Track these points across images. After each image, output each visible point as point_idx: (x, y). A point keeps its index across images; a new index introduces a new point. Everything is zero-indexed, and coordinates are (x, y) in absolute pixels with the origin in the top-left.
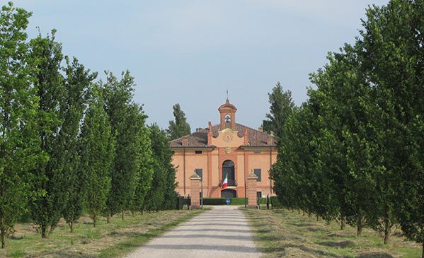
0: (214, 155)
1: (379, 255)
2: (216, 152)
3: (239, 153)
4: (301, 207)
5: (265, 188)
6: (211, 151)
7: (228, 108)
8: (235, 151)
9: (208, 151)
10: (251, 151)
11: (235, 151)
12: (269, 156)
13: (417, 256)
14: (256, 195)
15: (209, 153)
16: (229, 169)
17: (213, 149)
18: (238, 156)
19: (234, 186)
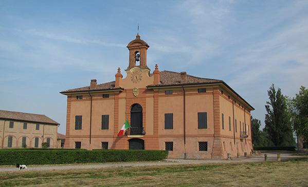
0: (121, 98)
1: (64, 171)
2: (123, 95)
3: (147, 95)
4: (91, 152)
5: (178, 137)
6: (118, 94)
7: (137, 44)
8: (144, 92)
9: (115, 94)
10: (161, 92)
11: (144, 92)
12: (183, 97)
13: (306, 186)
14: (208, 149)
15: (116, 96)
16: (136, 113)
17: (121, 92)
18: (147, 99)
19: (142, 134)
